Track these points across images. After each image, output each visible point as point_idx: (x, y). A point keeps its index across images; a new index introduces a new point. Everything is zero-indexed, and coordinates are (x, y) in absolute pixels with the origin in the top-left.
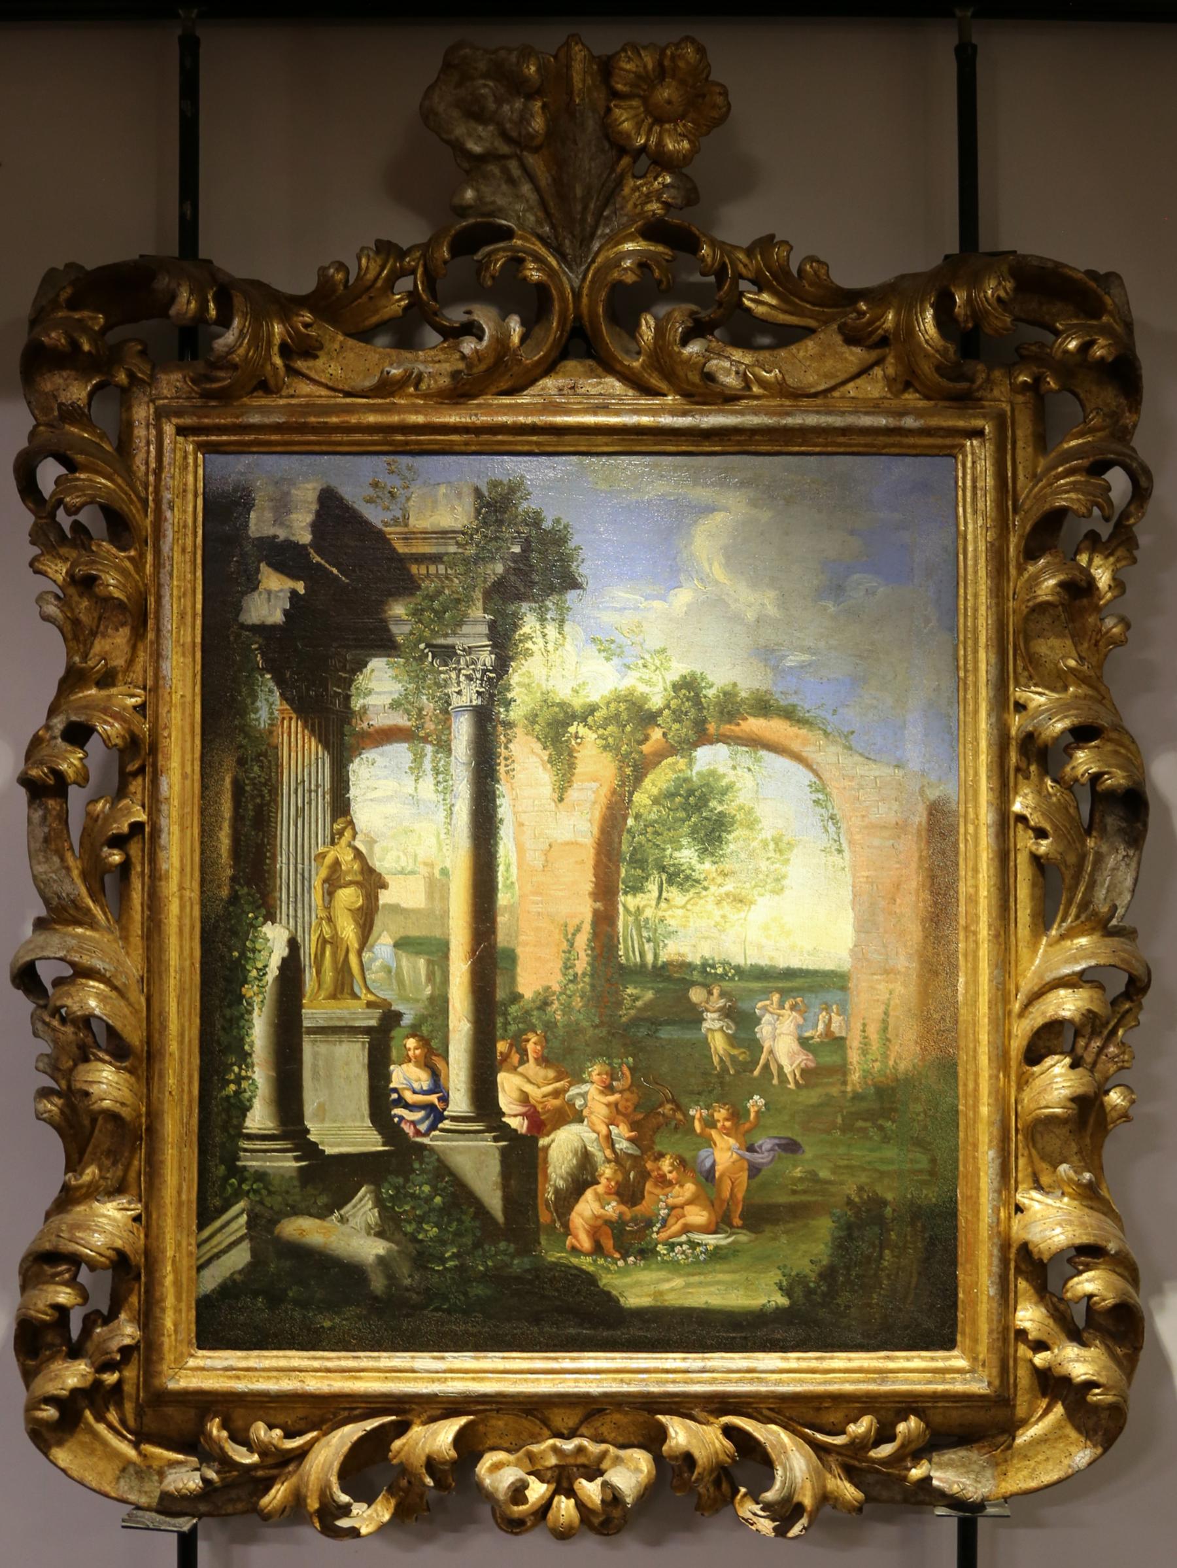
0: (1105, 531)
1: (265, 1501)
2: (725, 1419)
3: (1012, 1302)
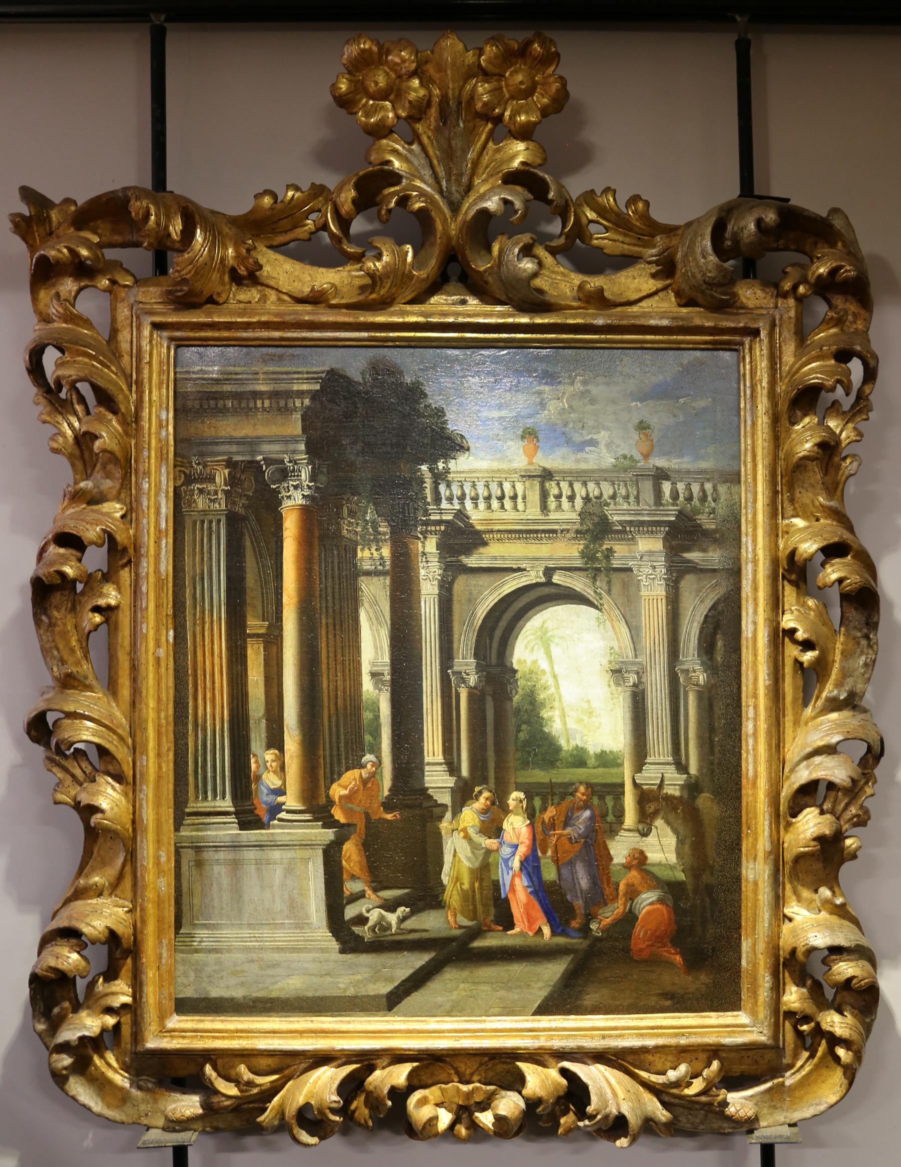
0: (847, 403)
1: (260, 1119)
2: (566, 1064)
3: (781, 990)
